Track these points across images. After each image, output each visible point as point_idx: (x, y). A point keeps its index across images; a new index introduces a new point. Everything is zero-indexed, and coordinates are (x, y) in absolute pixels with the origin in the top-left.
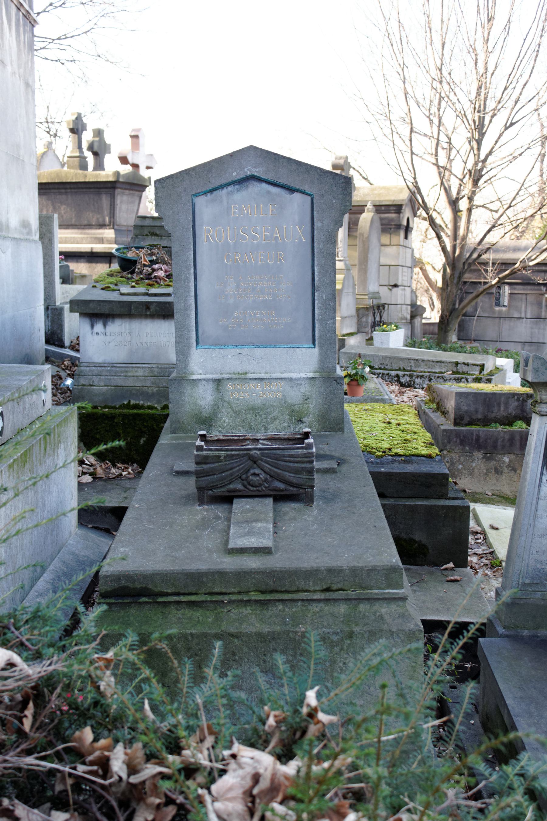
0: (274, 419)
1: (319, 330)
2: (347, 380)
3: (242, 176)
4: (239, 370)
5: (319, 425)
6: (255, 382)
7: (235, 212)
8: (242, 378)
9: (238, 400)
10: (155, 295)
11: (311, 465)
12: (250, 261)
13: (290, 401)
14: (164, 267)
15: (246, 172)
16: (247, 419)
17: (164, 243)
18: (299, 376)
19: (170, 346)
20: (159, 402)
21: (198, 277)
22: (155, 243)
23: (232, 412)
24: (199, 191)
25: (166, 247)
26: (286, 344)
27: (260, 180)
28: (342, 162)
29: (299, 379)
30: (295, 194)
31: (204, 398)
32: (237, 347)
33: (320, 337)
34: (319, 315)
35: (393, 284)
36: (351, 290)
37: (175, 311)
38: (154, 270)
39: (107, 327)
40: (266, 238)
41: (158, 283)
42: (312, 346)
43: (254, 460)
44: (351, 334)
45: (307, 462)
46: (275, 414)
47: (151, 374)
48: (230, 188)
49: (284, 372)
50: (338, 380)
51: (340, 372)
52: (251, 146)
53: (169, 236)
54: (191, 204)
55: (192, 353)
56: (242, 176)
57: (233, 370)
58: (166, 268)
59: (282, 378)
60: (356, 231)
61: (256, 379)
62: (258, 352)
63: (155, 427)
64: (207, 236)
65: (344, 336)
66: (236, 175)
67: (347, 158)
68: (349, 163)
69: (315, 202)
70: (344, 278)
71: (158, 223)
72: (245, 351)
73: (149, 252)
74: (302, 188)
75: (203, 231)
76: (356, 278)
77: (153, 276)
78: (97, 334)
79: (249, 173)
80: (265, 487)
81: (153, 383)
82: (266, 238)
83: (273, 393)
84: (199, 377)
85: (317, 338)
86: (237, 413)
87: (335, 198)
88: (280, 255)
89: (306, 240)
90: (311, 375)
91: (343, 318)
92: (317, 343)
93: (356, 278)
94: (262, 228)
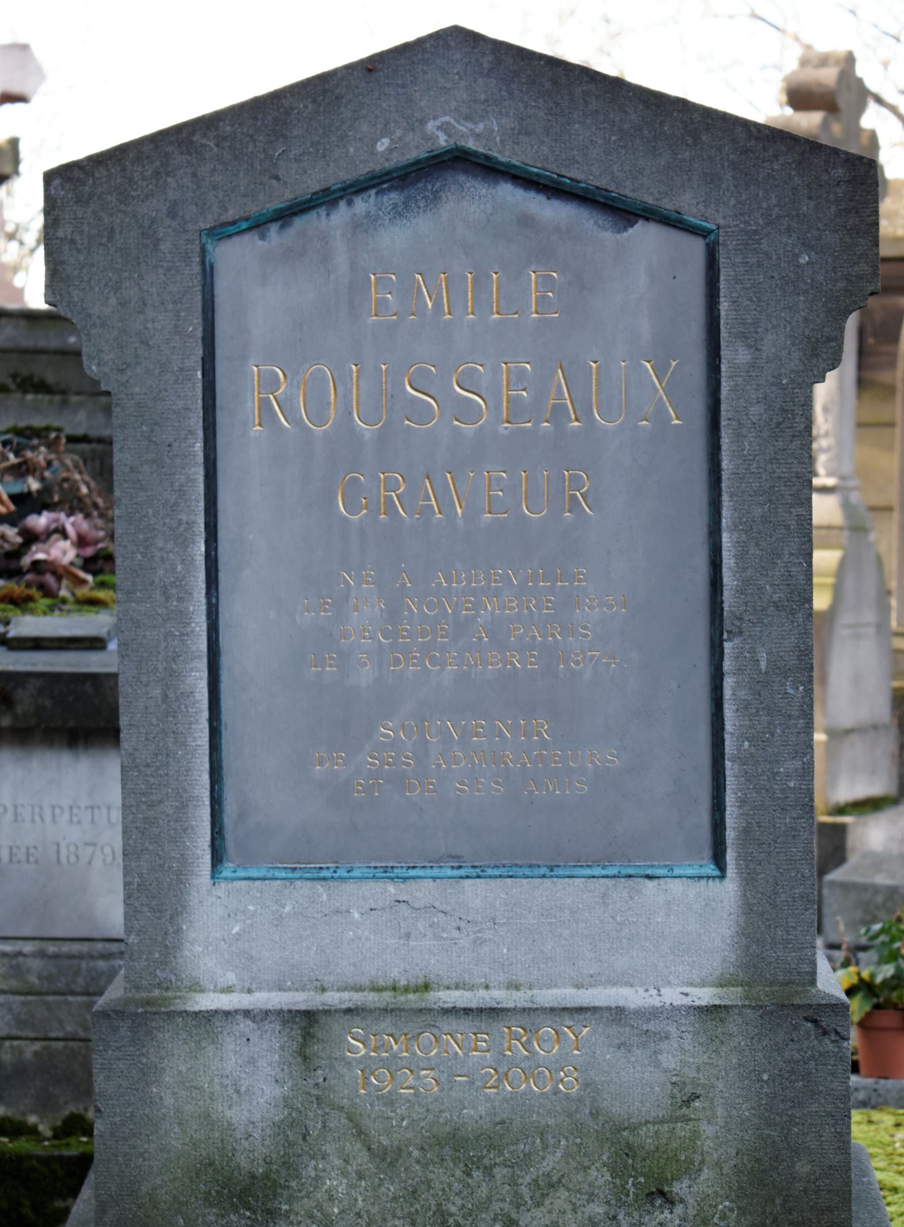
0: (547, 1186)
1: (742, 802)
2: (857, 1007)
3: (413, 155)
4: (397, 973)
5: (742, 1211)
6: (464, 1024)
7: (382, 304)
8: (407, 1007)
9: (391, 1101)
10: (37, 644)
12: (446, 507)
13: (616, 1109)
14: (73, 523)
15: (432, 138)
16: (428, 1183)
17: (78, 421)
18: (656, 1002)
19: (98, 863)
20: (45, 1104)
22: (38, 422)
23: (365, 1154)
24: (231, 214)
25: (85, 439)
26: (598, 863)
27: (490, 169)
28: (828, 76)
29: (653, 1013)
30: (640, 227)
31: (241, 1091)
32: (387, 874)
33: (746, 832)
34: (742, 738)
36: (870, 616)
37: (123, 721)
38: (31, 538)
40: (516, 410)
41: (48, 593)
42: (711, 869)
44: (870, 806)
46: (551, 1162)
47: (14, 983)
48: (362, 205)
49: (593, 981)
50: (822, 1017)
51: (832, 981)
52: (456, 31)
53: (97, 394)
54: (197, 269)
55: (193, 900)
57: (371, 971)
58: (85, 526)
59: (581, 1010)
60: (892, 364)
61: (467, 1011)
62: (477, 894)
63: (27, 1211)
64: (265, 405)
65: (841, 810)
66: (386, 149)
67: (850, 59)
68: (860, 82)
69: (722, 260)
70: (843, 563)
71: (50, 340)
72: (423, 891)
73: (12, 459)
74: (668, 205)
76: (892, 564)
77: (26, 561)
79: (443, 141)
81: (21, 1023)
82: (516, 410)
83: (549, 1072)
84: (225, 1002)
85: (730, 835)
86: (388, 1159)
87: (807, 246)
88: (576, 482)
89: (684, 418)
90: (705, 996)
91: (837, 735)
93: (892, 564)
94: (496, 370)
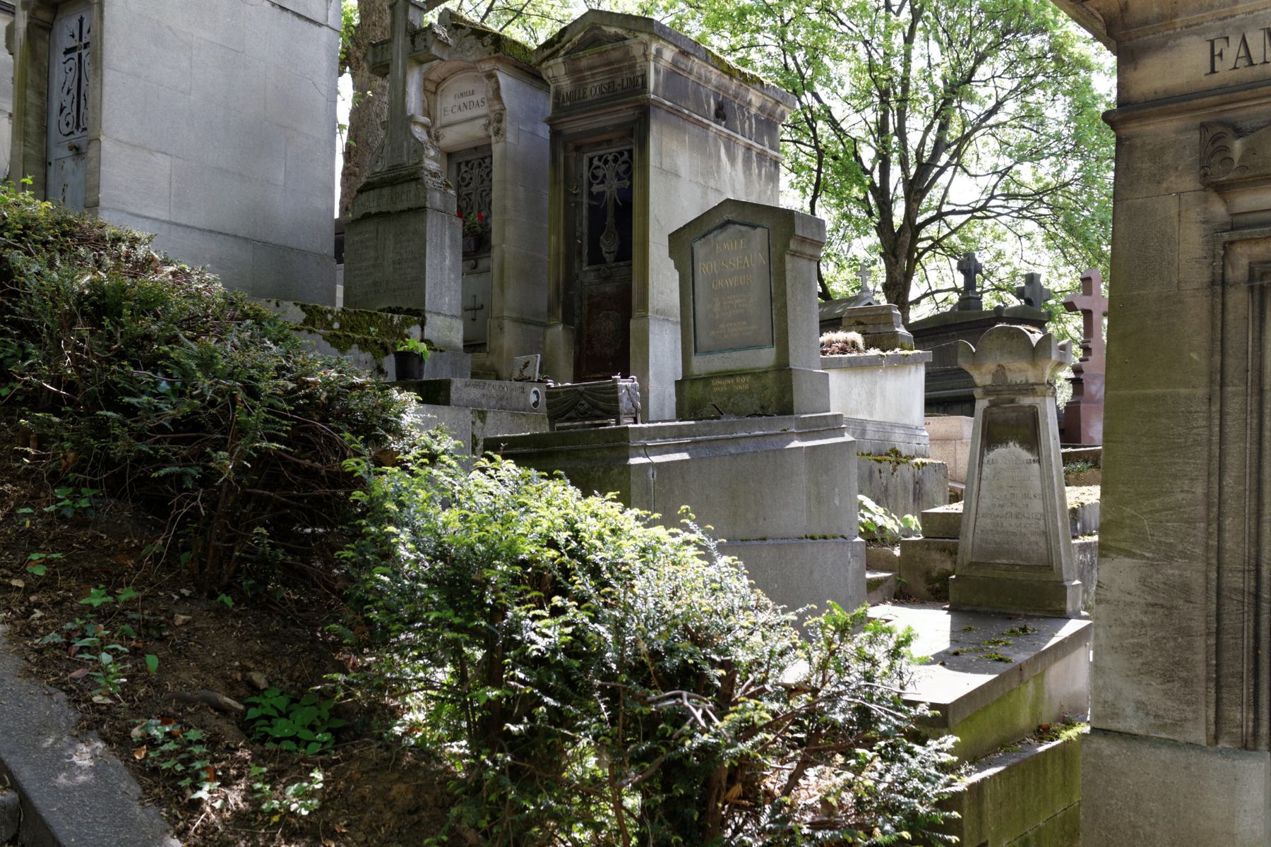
27: (734, 223)
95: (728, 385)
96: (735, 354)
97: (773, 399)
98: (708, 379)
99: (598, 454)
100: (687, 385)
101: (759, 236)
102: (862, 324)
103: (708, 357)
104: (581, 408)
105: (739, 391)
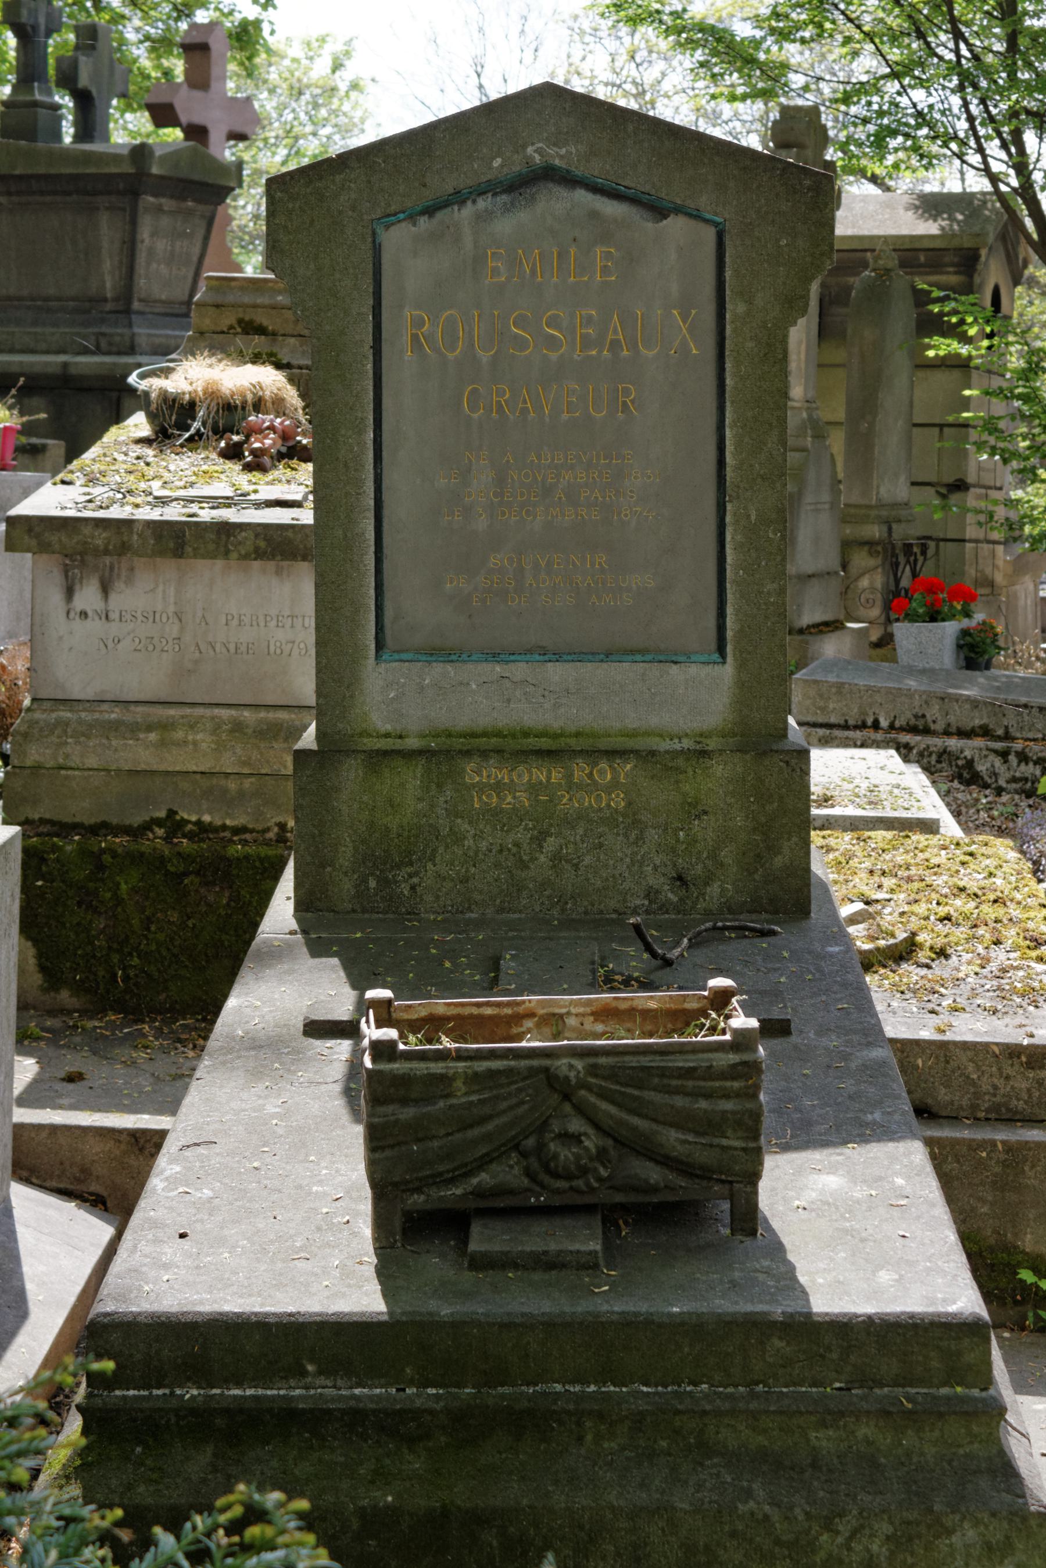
1: (737, 612)
7: (495, 271)
11: (749, 1105)
21: (385, 454)
24: (393, 208)
27: (569, 180)
35: (951, 480)
36: (826, 497)
39: (113, 597)
42: (716, 657)
43: (563, 1089)
45: (737, 1095)
54: (369, 245)
56: (517, 168)
69: (728, 242)
75: (402, 322)
78: (84, 614)
80: (600, 1179)
82: (587, 343)
88: (626, 392)
89: (701, 350)
92: (729, 649)
95: (534, 788)
96: (556, 672)
97: (727, 855)
98: (445, 754)
99: (824, 1440)
100: (351, 773)
101: (677, 246)
102: (261, 330)
103: (438, 671)
104: (565, 1154)
105: (582, 816)
